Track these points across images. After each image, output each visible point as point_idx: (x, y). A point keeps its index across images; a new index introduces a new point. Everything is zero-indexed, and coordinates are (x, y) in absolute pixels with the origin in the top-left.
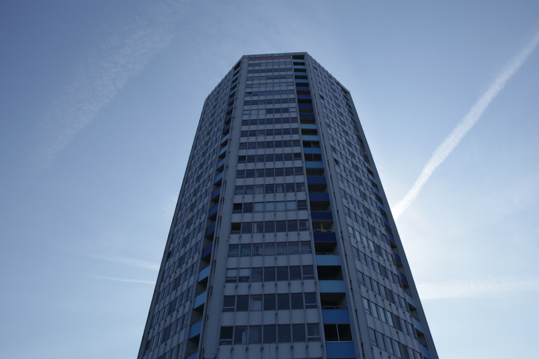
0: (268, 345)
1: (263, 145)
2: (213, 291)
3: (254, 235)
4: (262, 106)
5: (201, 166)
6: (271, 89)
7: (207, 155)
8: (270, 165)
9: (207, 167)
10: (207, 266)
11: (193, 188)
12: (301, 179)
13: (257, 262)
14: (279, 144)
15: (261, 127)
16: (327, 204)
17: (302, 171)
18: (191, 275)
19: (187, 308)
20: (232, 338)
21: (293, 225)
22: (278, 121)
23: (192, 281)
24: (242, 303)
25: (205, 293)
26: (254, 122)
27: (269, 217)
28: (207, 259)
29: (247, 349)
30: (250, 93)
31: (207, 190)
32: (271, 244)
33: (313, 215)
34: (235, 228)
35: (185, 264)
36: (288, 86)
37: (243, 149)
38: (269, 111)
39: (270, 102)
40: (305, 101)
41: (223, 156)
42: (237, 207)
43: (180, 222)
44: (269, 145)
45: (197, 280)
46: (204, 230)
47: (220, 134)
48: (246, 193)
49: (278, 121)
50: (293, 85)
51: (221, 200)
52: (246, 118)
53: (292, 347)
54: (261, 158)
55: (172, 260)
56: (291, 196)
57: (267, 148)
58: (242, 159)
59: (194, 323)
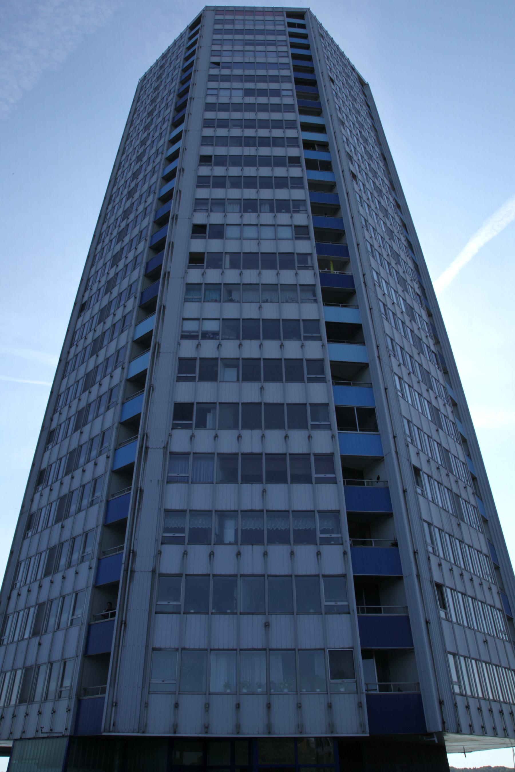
0: (249, 431)
1: (238, 141)
2: (161, 350)
3: (225, 271)
4: (237, 85)
5: (126, 214)
6: (252, 60)
7: (136, 196)
8: (250, 171)
9: (145, 176)
10: (143, 353)
11: (139, 140)
12: (300, 194)
13: (231, 311)
14: (264, 142)
15: (236, 115)
16: (339, 234)
17: (302, 183)
18: (122, 332)
19: (110, 419)
20: (191, 419)
21: (287, 261)
22: (263, 108)
23: (124, 339)
24: (208, 370)
25: (150, 353)
26: (224, 107)
27: (250, 247)
28: (148, 307)
29: (216, 436)
30: (218, 64)
31: (136, 258)
32: (253, 287)
33: (319, 249)
34: (196, 259)
35: (96, 386)
36: (279, 56)
37: (207, 145)
38: (248, 92)
39: (250, 78)
40: (307, 82)
41: (175, 156)
42: (199, 230)
43: (99, 260)
44: (249, 141)
45: (133, 338)
46: (144, 265)
47: (167, 125)
48: (211, 211)
49: (263, 108)
50: (288, 57)
51: (173, 218)
52: (211, 100)
53: (286, 437)
54: (236, 161)
55: (87, 315)
56: (283, 218)
57: (245, 146)
58: (205, 160)
59: (120, 445)
